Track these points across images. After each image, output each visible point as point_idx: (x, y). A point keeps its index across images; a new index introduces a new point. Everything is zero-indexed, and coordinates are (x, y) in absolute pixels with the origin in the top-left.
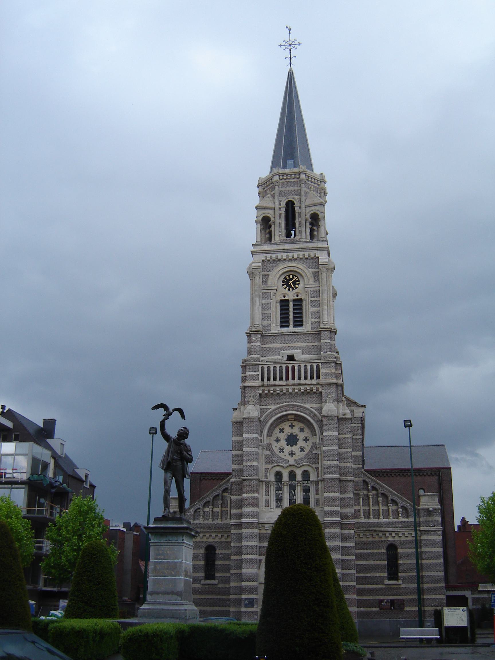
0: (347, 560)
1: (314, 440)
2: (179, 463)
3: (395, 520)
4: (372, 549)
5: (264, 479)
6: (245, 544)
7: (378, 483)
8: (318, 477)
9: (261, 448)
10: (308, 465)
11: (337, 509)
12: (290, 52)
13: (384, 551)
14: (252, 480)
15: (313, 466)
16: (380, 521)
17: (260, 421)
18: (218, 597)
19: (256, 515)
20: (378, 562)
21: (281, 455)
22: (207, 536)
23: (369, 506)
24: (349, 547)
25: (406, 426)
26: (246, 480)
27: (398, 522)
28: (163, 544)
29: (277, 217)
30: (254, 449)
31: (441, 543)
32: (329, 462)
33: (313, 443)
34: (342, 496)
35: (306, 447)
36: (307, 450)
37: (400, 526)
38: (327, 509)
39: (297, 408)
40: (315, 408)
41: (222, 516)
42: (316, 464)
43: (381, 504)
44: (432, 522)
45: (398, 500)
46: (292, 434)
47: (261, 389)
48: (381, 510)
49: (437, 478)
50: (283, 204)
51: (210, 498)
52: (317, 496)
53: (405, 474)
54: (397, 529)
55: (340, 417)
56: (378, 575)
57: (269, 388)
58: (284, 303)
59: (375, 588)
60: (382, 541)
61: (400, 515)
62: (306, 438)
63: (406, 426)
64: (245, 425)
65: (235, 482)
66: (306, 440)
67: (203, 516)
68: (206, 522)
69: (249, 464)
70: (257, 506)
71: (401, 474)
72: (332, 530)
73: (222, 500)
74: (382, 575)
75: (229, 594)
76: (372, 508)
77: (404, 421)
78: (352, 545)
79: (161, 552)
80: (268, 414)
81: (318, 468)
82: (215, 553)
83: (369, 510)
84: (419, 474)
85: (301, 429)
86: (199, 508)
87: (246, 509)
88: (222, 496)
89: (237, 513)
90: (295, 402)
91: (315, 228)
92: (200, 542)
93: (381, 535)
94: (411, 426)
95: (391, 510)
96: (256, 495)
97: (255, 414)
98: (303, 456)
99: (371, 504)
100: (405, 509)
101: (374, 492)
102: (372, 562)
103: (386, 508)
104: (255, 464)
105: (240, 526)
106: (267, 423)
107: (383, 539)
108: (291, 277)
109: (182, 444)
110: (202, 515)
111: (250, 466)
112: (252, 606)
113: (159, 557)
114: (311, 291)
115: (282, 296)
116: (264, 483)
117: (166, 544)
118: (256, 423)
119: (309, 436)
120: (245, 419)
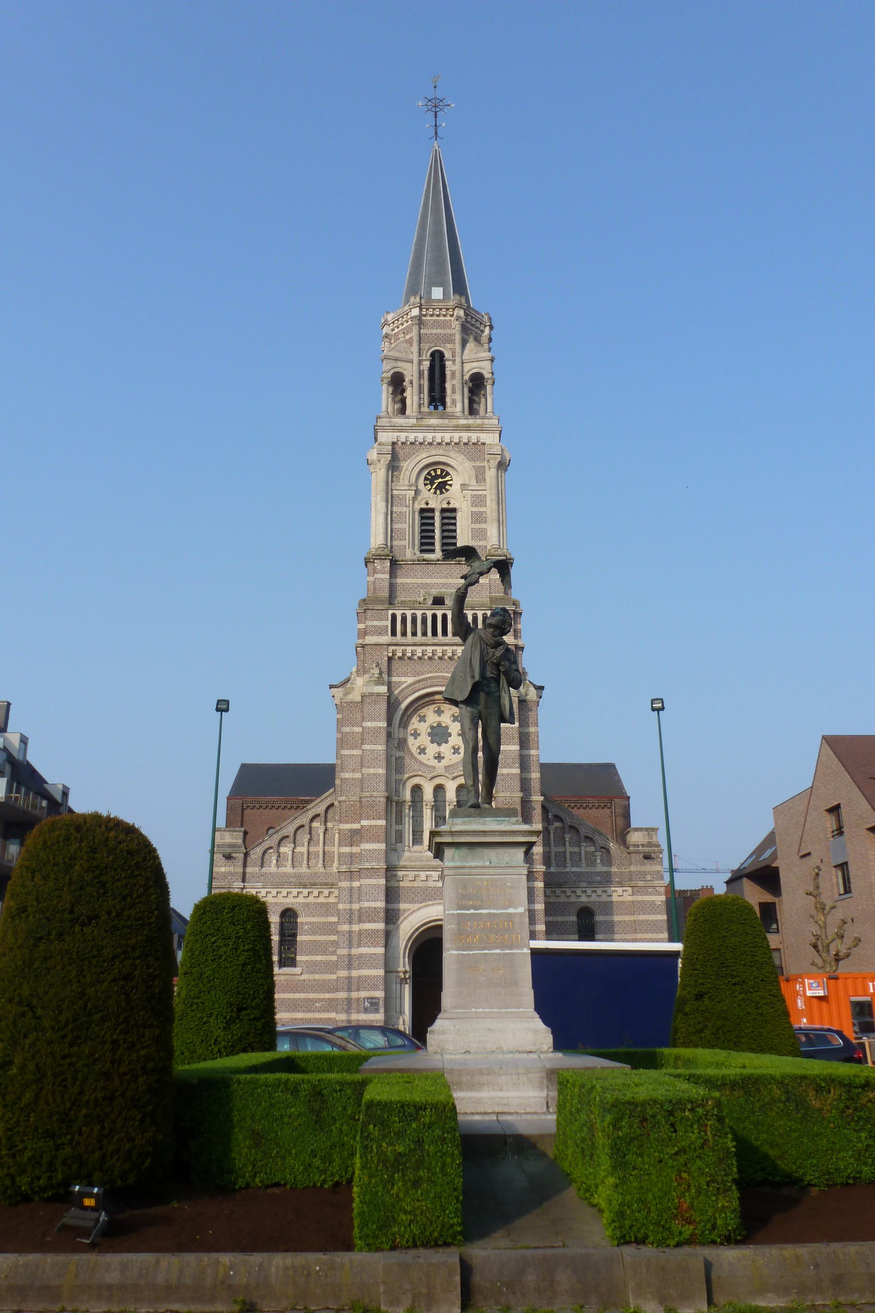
12: (436, 117)
13: (574, 918)
16: (568, 869)
18: (302, 996)
21: (421, 757)
29: (416, 375)
31: (664, 907)
43: (567, 843)
44: (650, 873)
46: (439, 725)
47: (391, 648)
48: (568, 854)
50: (427, 356)
57: (403, 648)
58: (426, 514)
61: (598, 861)
73: (310, 833)
82: (296, 923)
88: (310, 828)
91: (475, 398)
99: (552, 842)
101: (558, 824)
107: (573, 899)
108: (439, 472)
111: (374, 775)
114: (473, 496)
115: (423, 502)
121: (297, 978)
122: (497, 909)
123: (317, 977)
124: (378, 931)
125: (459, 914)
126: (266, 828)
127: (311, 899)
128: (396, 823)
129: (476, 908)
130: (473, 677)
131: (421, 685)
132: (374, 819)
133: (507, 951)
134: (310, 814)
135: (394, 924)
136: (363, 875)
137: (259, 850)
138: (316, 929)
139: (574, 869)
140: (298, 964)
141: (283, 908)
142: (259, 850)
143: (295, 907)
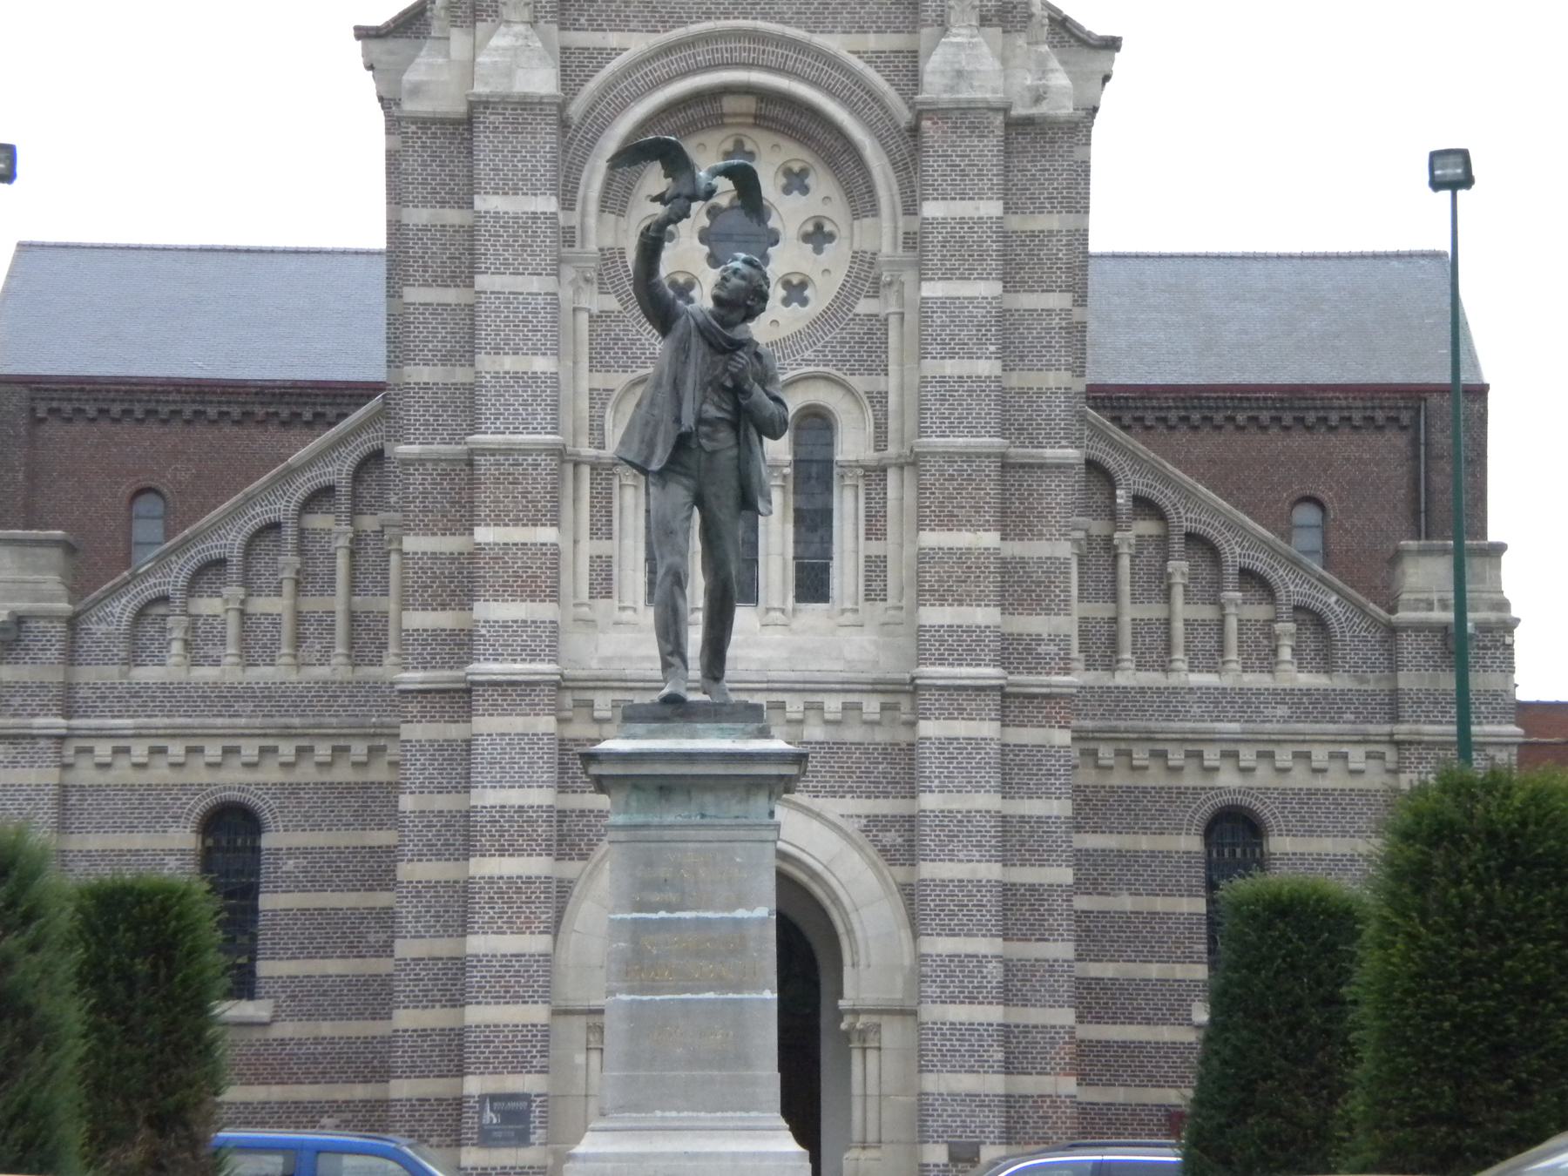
0: (1032, 888)
1: (864, 243)
2: (725, 437)
3: (1253, 680)
4: (1129, 830)
5: (587, 451)
6: (487, 797)
7: (1167, 480)
8: (880, 440)
9: (569, 273)
10: (827, 378)
11: (985, 615)
13: (1192, 843)
14: (526, 452)
15: (857, 382)
16: (1174, 680)
17: (564, 124)
19: (549, 639)
20: (1160, 904)
22: (213, 751)
23: (1115, 597)
24: (1040, 820)
25: (1436, 184)
26: (493, 452)
27: (1275, 692)
28: (676, 833)
30: (535, 284)
32: (951, 368)
33: (856, 256)
34: (1015, 549)
35: (817, 277)
36: (820, 297)
37: (1282, 711)
38: (936, 615)
39: (774, 54)
40: (874, 58)
41: (299, 640)
42: (870, 371)
43: (1178, 592)
45: (1279, 575)
48: (1178, 627)
49: (1401, 441)
51: (230, 542)
52: (875, 548)
53: (1219, 417)
54: (1268, 727)
55: (1014, 113)
56: (1154, 970)
59: (1141, 1045)
60: (1181, 792)
61: (1286, 653)
62: (819, 227)
63: (1436, 184)
64: (484, 142)
65: (422, 461)
66: (818, 236)
67: (186, 643)
68: (206, 673)
69: (508, 363)
70: (554, 595)
71: (1196, 416)
72: (960, 728)
73: (301, 551)
74: (1180, 971)
75: (383, 1073)
76: (1130, 612)
77: (1435, 156)
78: (1059, 808)
79: (663, 872)
80: (609, 86)
81: (885, 395)
82: (256, 850)
83: (1114, 620)
84: (1300, 420)
85: (788, 172)
86: (164, 599)
87: (493, 611)
88: (302, 532)
89: (435, 633)
90: (765, 16)
92: (167, 788)
93: (1176, 757)
94: (1467, 181)
95: (1232, 624)
96: (546, 534)
97: (541, 81)
98: (801, 325)
99: (1125, 589)
100: (1312, 619)
101: (1147, 527)
102: (1125, 902)
103: (1207, 613)
104: (542, 364)
105: (461, 699)
106: (601, 130)
107: (1191, 779)
109: (739, 345)
110: (178, 634)
111: (516, 376)
112: (522, 1139)
113: (656, 897)
116: (585, 471)
117: (691, 833)
118: (546, 139)
119: (836, 212)
120: (478, 106)
121: (257, 1034)
122: (715, 909)
123: (327, 1029)
124: (529, 881)
125: (635, 920)
126: (125, 490)
127: (307, 773)
128: (593, 534)
129: (670, 908)
130: (678, 420)
131: (675, 61)
132: (517, 522)
133: (731, 996)
134: (303, 486)
135: (583, 857)
136: (480, 704)
137: (122, 609)
138: (324, 869)
139: (1197, 679)
140: (262, 987)
141: (209, 802)
142: (122, 609)
143: (252, 800)
